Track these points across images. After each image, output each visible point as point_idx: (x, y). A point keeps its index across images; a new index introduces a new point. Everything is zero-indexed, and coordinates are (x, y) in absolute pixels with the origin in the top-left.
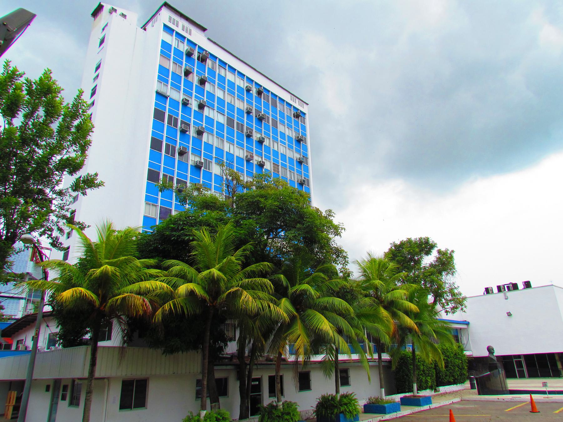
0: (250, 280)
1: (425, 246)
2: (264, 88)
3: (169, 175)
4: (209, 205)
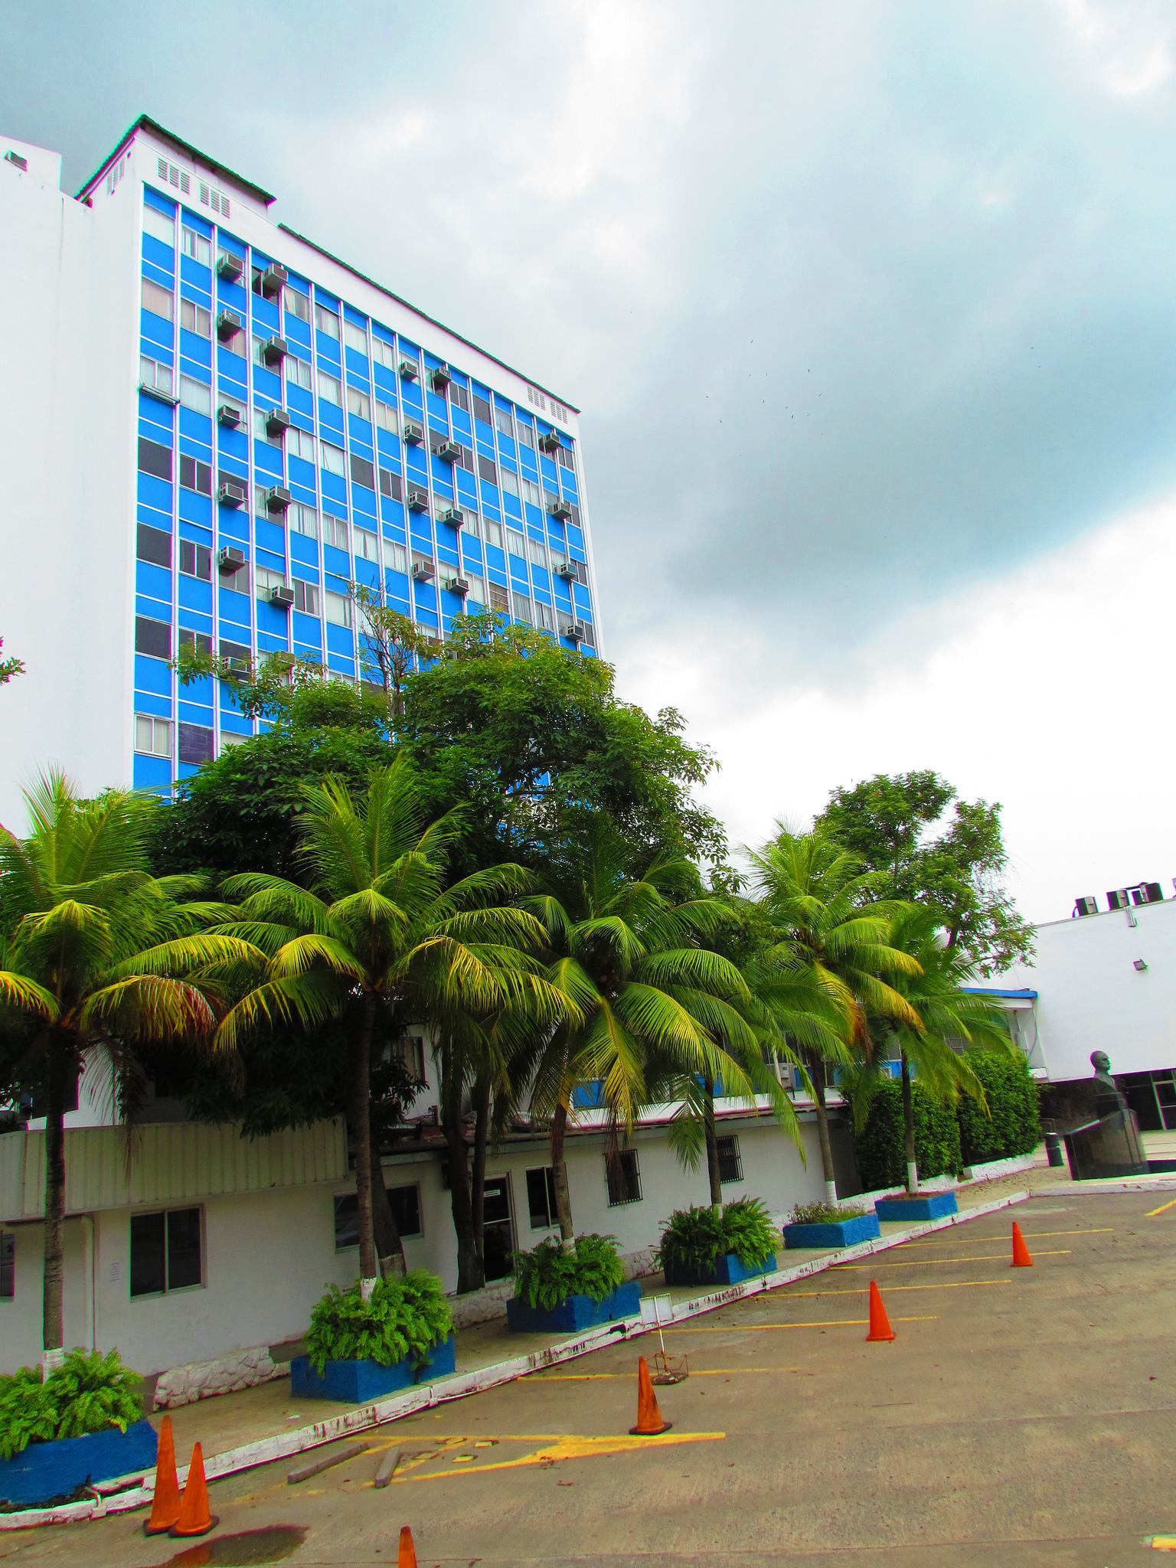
0: (476, 914)
1: (925, 795)
2: (451, 367)
3: (196, 632)
4: (326, 711)
